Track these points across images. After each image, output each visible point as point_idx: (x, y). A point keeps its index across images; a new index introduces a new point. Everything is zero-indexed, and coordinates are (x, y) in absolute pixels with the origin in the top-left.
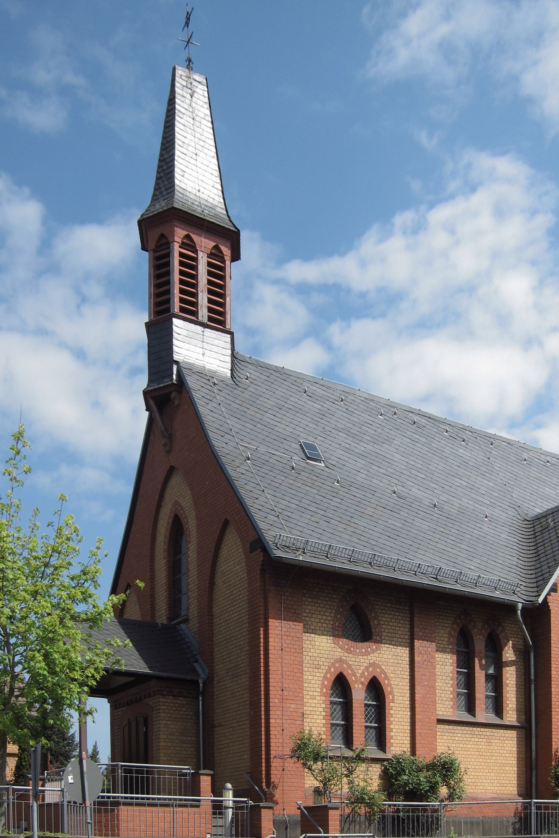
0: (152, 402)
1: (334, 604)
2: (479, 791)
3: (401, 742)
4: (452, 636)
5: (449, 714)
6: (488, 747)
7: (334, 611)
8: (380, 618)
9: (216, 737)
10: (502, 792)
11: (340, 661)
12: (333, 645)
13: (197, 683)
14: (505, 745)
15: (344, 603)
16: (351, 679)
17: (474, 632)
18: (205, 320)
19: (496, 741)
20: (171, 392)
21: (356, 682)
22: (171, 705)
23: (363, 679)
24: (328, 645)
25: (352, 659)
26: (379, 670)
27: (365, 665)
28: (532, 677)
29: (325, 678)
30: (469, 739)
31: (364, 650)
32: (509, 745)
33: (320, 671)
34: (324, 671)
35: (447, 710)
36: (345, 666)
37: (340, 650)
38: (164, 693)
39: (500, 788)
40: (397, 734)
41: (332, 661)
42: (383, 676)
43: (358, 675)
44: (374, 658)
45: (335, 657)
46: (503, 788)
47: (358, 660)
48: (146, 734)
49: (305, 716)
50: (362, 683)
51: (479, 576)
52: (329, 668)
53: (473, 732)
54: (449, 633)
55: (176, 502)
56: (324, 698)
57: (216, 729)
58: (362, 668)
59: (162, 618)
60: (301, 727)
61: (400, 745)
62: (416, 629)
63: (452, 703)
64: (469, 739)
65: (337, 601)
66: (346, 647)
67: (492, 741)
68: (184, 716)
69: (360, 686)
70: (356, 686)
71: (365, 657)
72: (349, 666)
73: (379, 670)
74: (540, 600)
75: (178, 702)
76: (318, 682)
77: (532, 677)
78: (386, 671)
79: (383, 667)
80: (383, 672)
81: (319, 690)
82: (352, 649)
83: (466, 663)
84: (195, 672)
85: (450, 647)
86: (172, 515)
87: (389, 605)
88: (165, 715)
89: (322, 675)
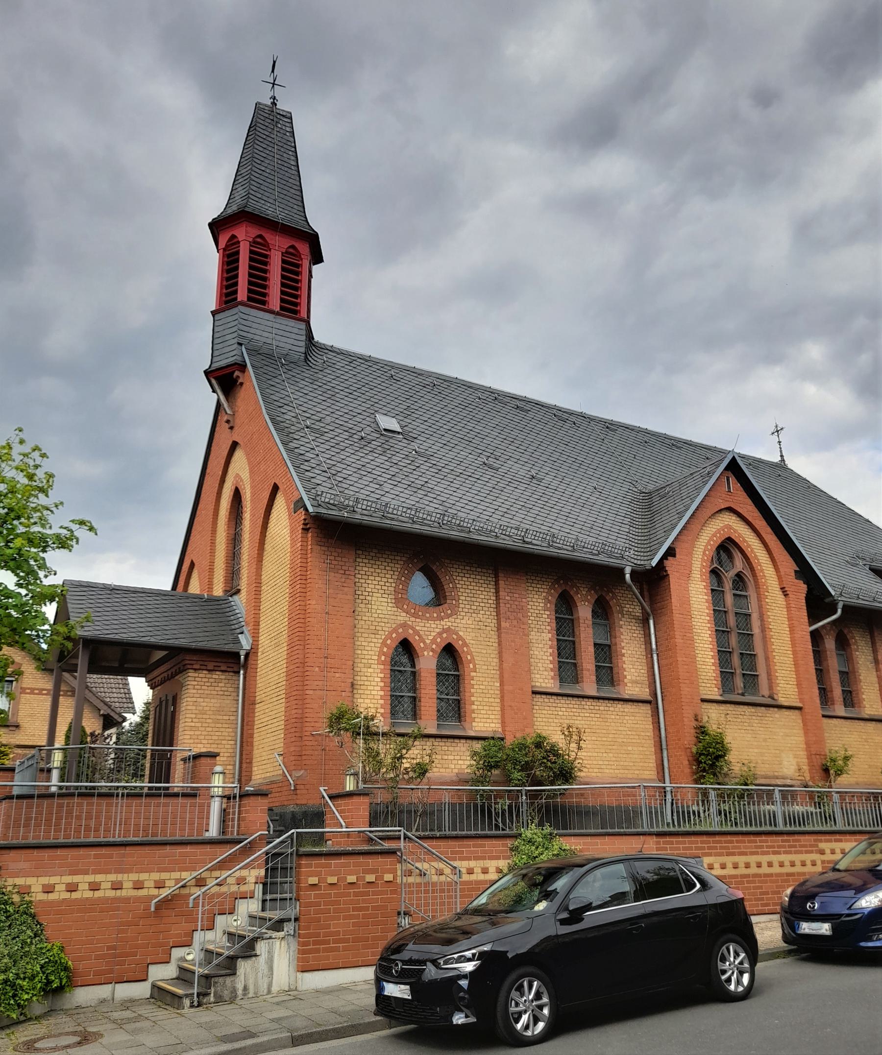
0: (214, 381)
1: (397, 566)
2: (593, 774)
3: (485, 716)
4: (550, 602)
5: (549, 685)
6: (603, 724)
7: (397, 573)
8: (457, 582)
9: (257, 714)
10: (624, 776)
11: (404, 625)
12: (396, 609)
13: (237, 655)
14: (625, 721)
15: (410, 565)
16: (419, 646)
17: (577, 598)
18: (278, 309)
19: (613, 717)
20: (234, 372)
21: (424, 649)
22: (204, 680)
23: (434, 646)
24: (389, 609)
25: (420, 626)
26: (455, 637)
27: (438, 630)
28: (654, 646)
29: (384, 643)
30: (577, 714)
31: (435, 615)
32: (630, 722)
33: (379, 637)
34: (383, 637)
35: (546, 681)
36: (411, 631)
37: (404, 614)
38: (195, 667)
39: (622, 771)
40: (480, 707)
41: (394, 626)
42: (460, 642)
43: (428, 642)
44: (450, 624)
45: (399, 622)
46: (626, 772)
47: (428, 625)
48: (174, 713)
49: (356, 687)
50: (433, 650)
51: (577, 540)
52: (391, 633)
53: (581, 707)
54: (545, 598)
55: (237, 475)
56: (382, 667)
57: (257, 706)
58: (433, 634)
59: (218, 591)
60: (350, 699)
61: (484, 720)
62: (502, 593)
63: (552, 674)
64: (577, 714)
65: (402, 563)
66: (413, 611)
67: (608, 716)
68: (222, 693)
69: (431, 654)
70: (426, 653)
71: (438, 622)
72: (417, 633)
73: (455, 637)
74: (654, 563)
75: (214, 676)
76: (376, 649)
77: (654, 646)
78: (464, 637)
79: (461, 633)
80: (460, 638)
81: (376, 658)
82: (420, 613)
83: (565, 627)
84: (238, 642)
85: (548, 613)
86: (234, 488)
87: (468, 568)
88: (195, 691)
89: (381, 641)
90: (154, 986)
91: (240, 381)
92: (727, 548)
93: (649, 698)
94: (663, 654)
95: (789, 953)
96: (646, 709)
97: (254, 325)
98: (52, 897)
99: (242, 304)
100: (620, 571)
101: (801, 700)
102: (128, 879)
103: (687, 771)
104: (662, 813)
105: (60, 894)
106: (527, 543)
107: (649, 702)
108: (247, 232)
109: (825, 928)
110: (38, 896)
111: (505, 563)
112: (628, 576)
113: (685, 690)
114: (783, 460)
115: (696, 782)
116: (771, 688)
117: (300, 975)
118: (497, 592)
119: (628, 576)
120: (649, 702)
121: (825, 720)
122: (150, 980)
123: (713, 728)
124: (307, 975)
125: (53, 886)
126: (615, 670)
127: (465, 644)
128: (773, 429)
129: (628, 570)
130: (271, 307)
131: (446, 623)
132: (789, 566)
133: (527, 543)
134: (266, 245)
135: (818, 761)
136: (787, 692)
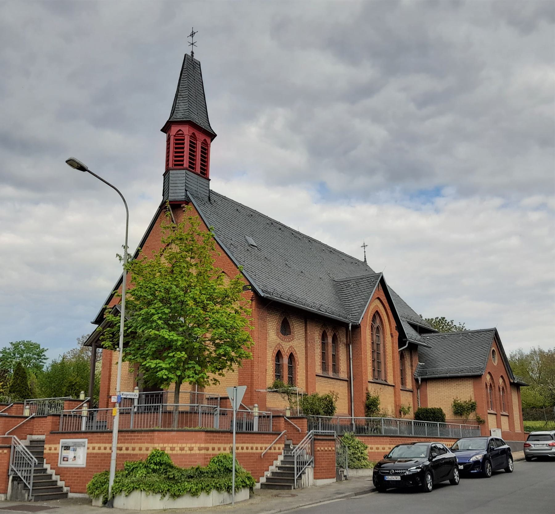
16: (283, 353)
17: (328, 334)
90: (262, 484)
91: (184, 209)
92: (377, 314)
93: (347, 379)
94: (354, 359)
95: (373, 490)
96: (346, 384)
97: (191, 181)
98: (193, 452)
99: (186, 169)
100: (348, 324)
101: (394, 383)
102: (187, 446)
103: (363, 411)
104: (135, 424)
105: (177, 451)
106: (282, 298)
107: (347, 381)
108: (189, 131)
109: (398, 478)
110: (168, 451)
111: (308, 317)
112: (350, 327)
113: (364, 377)
114: (365, 261)
115: (366, 416)
116: (386, 377)
117: (315, 480)
118: (306, 330)
119: (350, 327)
120: (347, 381)
121: (401, 392)
122: (260, 482)
123: (373, 394)
124: (318, 481)
125: (175, 448)
126: (337, 366)
127: (296, 353)
128: (362, 245)
129: (350, 325)
130: (197, 171)
131: (291, 344)
132: (394, 324)
133: (282, 298)
134: (195, 139)
135: (398, 409)
136: (390, 381)
